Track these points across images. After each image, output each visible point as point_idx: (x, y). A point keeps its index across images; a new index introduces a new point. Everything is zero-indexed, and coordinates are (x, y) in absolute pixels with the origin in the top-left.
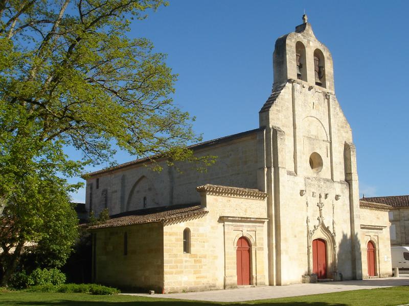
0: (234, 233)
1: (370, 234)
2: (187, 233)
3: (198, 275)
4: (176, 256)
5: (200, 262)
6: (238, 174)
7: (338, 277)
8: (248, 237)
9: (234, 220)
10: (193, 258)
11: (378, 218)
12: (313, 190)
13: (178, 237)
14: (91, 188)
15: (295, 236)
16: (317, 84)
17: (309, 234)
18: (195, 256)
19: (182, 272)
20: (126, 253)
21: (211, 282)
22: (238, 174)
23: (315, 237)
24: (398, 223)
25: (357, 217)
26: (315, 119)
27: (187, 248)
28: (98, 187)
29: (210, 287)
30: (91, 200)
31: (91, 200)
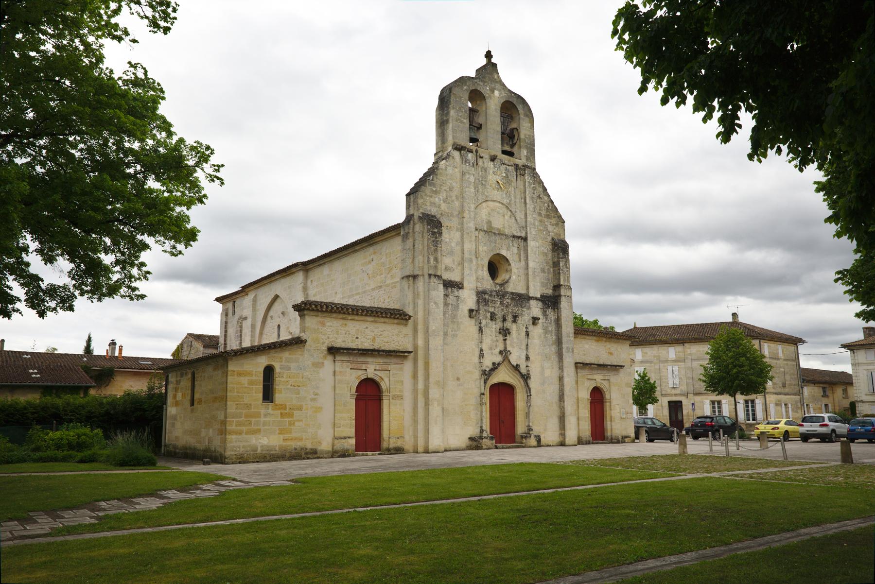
0: (350, 377)
1: (595, 377)
2: (269, 372)
3: (287, 436)
4: (248, 406)
5: (291, 415)
6: (381, 287)
7: (533, 441)
8: (377, 379)
9: (348, 351)
10: (279, 409)
11: (611, 354)
12: (492, 310)
13: (254, 378)
14: (227, 315)
15: (458, 379)
16: (504, 152)
17: (487, 374)
18: (283, 407)
19: (259, 431)
20: (192, 404)
21: (309, 446)
22: (381, 287)
23: (495, 379)
24: (682, 364)
25: (568, 351)
26: (500, 205)
27: (268, 395)
28: (234, 313)
29: (306, 453)
30: (226, 331)
31: (226, 331)
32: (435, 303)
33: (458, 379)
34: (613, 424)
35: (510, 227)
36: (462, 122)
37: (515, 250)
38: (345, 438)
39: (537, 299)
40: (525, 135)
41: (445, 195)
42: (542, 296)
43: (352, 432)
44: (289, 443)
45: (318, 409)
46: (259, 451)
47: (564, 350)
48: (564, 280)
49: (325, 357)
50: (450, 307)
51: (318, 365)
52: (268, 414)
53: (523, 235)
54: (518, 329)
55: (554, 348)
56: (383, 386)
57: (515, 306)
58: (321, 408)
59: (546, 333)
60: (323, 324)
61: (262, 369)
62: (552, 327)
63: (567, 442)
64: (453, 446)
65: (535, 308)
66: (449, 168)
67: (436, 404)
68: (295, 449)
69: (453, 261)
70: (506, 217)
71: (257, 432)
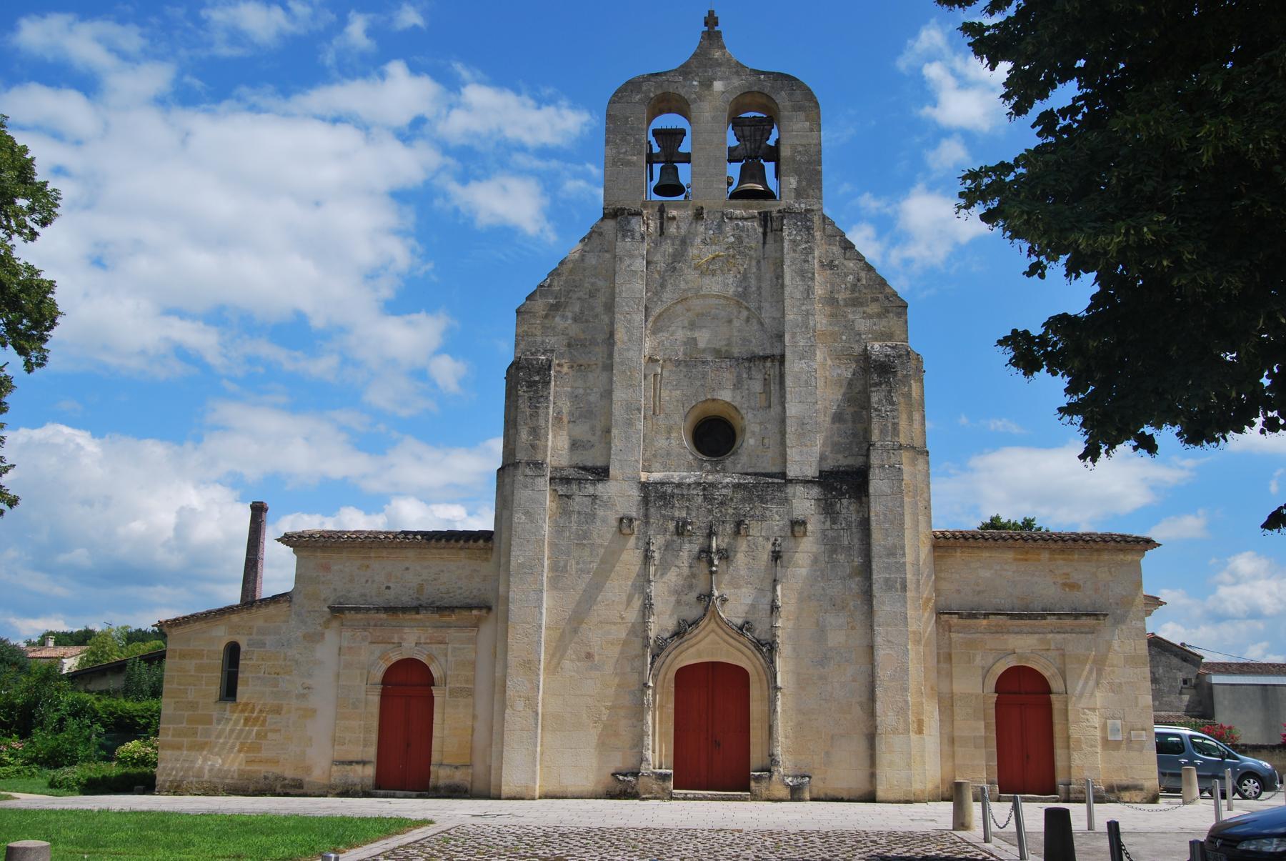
0: (374, 660)
2: (233, 652)
4: (193, 706)
21: (289, 773)
26: (722, 301)
29: (284, 786)
32: (527, 513)
33: (589, 656)
34: (1075, 755)
35: (745, 341)
36: (628, 163)
37: (757, 386)
38: (351, 763)
39: (806, 482)
40: (794, 147)
41: (577, 309)
42: (822, 474)
43: (371, 753)
44: (255, 767)
45: (310, 713)
46: (206, 777)
47: (876, 588)
48: (883, 432)
49: (327, 624)
50: (574, 517)
51: (314, 638)
52: (231, 721)
53: (777, 352)
54: (752, 549)
55: (855, 584)
56: (436, 671)
57: (743, 500)
58: (314, 711)
59: (835, 551)
60: (327, 568)
61: (222, 647)
62: (850, 538)
63: (880, 793)
64: (572, 789)
65: (804, 503)
66: (589, 256)
67: (520, 705)
68: (266, 778)
69: (593, 428)
70: (736, 323)
71: (201, 747)
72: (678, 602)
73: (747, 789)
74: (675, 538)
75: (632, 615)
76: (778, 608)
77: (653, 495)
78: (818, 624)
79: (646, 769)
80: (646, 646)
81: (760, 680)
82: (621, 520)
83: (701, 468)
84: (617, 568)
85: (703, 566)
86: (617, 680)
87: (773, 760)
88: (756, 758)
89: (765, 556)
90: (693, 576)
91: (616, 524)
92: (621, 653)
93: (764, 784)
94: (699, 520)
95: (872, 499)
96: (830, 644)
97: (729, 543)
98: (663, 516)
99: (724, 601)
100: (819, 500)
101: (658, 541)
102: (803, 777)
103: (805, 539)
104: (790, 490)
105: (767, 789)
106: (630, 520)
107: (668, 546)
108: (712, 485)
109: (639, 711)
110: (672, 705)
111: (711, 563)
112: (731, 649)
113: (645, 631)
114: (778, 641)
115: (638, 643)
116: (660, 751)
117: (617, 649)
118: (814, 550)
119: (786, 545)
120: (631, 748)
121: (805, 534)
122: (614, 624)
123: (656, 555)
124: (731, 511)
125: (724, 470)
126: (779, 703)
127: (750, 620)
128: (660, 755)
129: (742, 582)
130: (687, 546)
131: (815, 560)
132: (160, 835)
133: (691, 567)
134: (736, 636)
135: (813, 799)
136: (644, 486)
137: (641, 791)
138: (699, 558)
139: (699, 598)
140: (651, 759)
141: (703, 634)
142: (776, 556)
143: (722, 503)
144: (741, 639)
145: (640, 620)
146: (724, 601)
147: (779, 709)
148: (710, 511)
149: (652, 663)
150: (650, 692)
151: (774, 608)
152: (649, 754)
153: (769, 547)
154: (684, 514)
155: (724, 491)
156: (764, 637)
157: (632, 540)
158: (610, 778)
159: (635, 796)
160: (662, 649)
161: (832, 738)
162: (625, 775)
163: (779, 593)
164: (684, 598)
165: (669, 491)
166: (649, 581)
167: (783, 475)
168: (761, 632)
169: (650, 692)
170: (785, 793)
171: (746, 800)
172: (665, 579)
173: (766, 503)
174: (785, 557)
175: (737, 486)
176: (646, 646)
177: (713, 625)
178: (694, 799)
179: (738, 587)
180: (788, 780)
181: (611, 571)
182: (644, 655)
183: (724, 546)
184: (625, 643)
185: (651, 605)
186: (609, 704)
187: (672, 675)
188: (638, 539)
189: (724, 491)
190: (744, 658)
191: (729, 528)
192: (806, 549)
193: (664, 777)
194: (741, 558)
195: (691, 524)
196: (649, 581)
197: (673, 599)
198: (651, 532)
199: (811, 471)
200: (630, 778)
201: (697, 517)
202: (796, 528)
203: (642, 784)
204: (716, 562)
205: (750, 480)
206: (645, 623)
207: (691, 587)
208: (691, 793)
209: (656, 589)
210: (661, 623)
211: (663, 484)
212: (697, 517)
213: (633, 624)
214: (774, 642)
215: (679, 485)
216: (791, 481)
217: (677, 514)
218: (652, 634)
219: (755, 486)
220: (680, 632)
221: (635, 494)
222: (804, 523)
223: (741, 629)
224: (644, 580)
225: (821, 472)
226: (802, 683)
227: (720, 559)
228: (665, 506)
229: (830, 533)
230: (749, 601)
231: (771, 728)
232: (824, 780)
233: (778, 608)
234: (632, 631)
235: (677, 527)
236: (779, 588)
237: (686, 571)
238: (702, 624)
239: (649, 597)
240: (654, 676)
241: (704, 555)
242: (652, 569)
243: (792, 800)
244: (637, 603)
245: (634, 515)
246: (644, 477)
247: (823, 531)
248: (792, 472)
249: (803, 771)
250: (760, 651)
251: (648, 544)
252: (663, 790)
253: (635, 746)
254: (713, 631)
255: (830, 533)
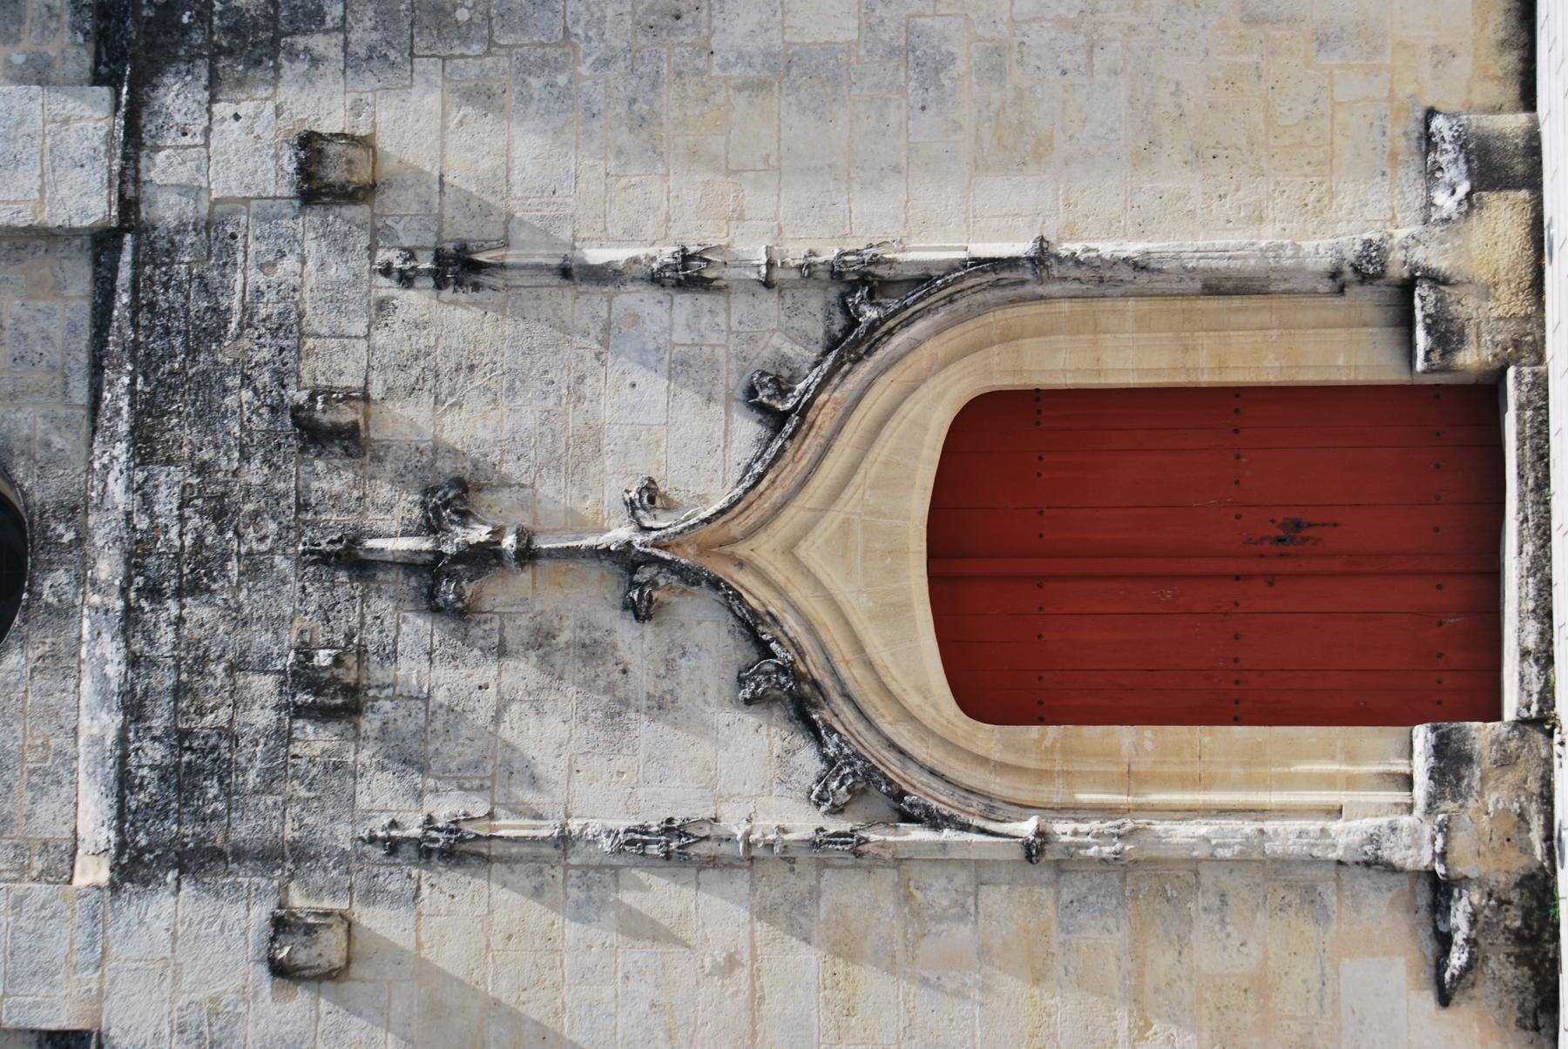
39: (134, 139)
54: (430, 377)
57: (208, 417)
72: (660, 706)
73: (1484, 395)
74: (369, 724)
75: (714, 914)
76: (686, 258)
77: (171, 830)
78: (761, 86)
79: (1414, 848)
80: (854, 845)
81: (1007, 336)
82: (281, 971)
83: (64, 613)
84: (503, 990)
85: (502, 594)
86: (1012, 986)
87: (1361, 273)
88: (1350, 353)
89: (458, 319)
90: (542, 640)
91: (301, 1000)
92: (891, 968)
93: (1467, 307)
94: (289, 613)
95: (524, 899)
96: (848, 31)
97: (399, 479)
98: (270, 780)
99: (651, 495)
100: (214, 84)
101: (386, 801)
102: (1428, 142)
103: (384, 143)
104: (166, 209)
105: (1488, 291)
106: (281, 924)
107: (409, 759)
108: (137, 555)
109: (1147, 880)
110: (1124, 736)
111: (483, 558)
112: (871, 469)
113: (788, 857)
114: (829, 253)
115: (847, 893)
116: (1329, 782)
117: (872, 983)
118: (432, 101)
119: (411, 230)
120: (1322, 916)
121: (365, 143)
122: (756, 1000)
123: (446, 808)
124: (255, 473)
125: (74, 510)
126: (1107, 249)
127: (739, 386)
128: (1352, 783)
129: (575, 420)
130: (409, 670)
131: (481, 96)
132: (99, 945)
133: (502, 651)
134: (812, 444)
135: (1528, 98)
136: (133, 868)
137: (1517, 864)
138: (462, 615)
139: (641, 611)
140: (1367, 824)
141: (801, 593)
142: (458, 268)
143: (220, 512)
144: (823, 418)
145: (741, 882)
146: (651, 495)
147: (1132, 248)
148: (254, 567)
149: (935, 820)
150: (1063, 829)
151: (688, 275)
152: (1347, 835)
153: (417, 301)
154: (264, 685)
155: (167, 503)
156: (813, 316)
157: (376, 920)
158: (1463, 1014)
159: (1539, 890)
160: (871, 775)
161: (1252, 20)
162: (1444, 941)
163: (617, 255)
164: (642, 680)
165: (155, 753)
166: (564, 841)
167: (103, 242)
168: (790, 335)
169: (1063, 829)
170: (1503, 214)
171: (1541, 385)
172: (547, 763)
173: (222, 315)
174: (461, 229)
175: (146, 447)
176: (854, 845)
177: (763, 549)
178: (1544, 614)
179: (593, 438)
180: (1446, 202)
181: (514, 1017)
182: (900, 860)
183: (408, 505)
184: (845, 949)
185: (669, 828)
186: (1123, 1019)
187: (988, 738)
188: (370, 896)
189: (167, 503)
190: (911, 408)
191: (330, 479)
192: (421, 128)
193: (1451, 763)
194: (468, 428)
195: (305, 651)
196: (564, 841)
197: (646, 730)
198: (343, 835)
199: (90, 117)
200: (1459, 918)
201: (276, 624)
202: (334, 174)
203: (1483, 858)
204: (479, 534)
205: (118, 390)
206: (752, 858)
207: (591, 650)
208: (1516, 632)
209: (601, 804)
210: (753, 778)
211: (125, 782)
212: (276, 624)
213: (764, 913)
214: (835, 273)
215: (134, 707)
216: (128, 206)
217: (262, 717)
218: (804, 822)
219: (146, 364)
220: (791, 692)
221: (167, 907)
222: (310, 144)
223: (776, 420)
224: (553, 859)
225: (97, 80)
226: (1018, 146)
227: (465, 517)
228: (225, 771)
229: (363, 34)
230: (655, 386)
231: (1218, 286)
232: (1442, 55)
233: (686, 258)
234: (791, 915)
235: (322, 714)
236: (596, 255)
237: (520, 672)
238: (758, 595)
239: (635, 842)
240: (989, 813)
241: (448, 590)
242: (508, 826)
243: (1533, 180)
244: (658, 894)
245: (261, 913)
246: (93, 871)
247: (352, 63)
248: (87, 202)
249: (1406, 146)
250: (875, 336)
251: (393, 847)
252: (1506, 761)
253: (1310, 895)
254: (789, 550)
255: (363, 34)
